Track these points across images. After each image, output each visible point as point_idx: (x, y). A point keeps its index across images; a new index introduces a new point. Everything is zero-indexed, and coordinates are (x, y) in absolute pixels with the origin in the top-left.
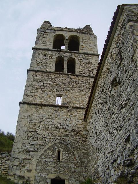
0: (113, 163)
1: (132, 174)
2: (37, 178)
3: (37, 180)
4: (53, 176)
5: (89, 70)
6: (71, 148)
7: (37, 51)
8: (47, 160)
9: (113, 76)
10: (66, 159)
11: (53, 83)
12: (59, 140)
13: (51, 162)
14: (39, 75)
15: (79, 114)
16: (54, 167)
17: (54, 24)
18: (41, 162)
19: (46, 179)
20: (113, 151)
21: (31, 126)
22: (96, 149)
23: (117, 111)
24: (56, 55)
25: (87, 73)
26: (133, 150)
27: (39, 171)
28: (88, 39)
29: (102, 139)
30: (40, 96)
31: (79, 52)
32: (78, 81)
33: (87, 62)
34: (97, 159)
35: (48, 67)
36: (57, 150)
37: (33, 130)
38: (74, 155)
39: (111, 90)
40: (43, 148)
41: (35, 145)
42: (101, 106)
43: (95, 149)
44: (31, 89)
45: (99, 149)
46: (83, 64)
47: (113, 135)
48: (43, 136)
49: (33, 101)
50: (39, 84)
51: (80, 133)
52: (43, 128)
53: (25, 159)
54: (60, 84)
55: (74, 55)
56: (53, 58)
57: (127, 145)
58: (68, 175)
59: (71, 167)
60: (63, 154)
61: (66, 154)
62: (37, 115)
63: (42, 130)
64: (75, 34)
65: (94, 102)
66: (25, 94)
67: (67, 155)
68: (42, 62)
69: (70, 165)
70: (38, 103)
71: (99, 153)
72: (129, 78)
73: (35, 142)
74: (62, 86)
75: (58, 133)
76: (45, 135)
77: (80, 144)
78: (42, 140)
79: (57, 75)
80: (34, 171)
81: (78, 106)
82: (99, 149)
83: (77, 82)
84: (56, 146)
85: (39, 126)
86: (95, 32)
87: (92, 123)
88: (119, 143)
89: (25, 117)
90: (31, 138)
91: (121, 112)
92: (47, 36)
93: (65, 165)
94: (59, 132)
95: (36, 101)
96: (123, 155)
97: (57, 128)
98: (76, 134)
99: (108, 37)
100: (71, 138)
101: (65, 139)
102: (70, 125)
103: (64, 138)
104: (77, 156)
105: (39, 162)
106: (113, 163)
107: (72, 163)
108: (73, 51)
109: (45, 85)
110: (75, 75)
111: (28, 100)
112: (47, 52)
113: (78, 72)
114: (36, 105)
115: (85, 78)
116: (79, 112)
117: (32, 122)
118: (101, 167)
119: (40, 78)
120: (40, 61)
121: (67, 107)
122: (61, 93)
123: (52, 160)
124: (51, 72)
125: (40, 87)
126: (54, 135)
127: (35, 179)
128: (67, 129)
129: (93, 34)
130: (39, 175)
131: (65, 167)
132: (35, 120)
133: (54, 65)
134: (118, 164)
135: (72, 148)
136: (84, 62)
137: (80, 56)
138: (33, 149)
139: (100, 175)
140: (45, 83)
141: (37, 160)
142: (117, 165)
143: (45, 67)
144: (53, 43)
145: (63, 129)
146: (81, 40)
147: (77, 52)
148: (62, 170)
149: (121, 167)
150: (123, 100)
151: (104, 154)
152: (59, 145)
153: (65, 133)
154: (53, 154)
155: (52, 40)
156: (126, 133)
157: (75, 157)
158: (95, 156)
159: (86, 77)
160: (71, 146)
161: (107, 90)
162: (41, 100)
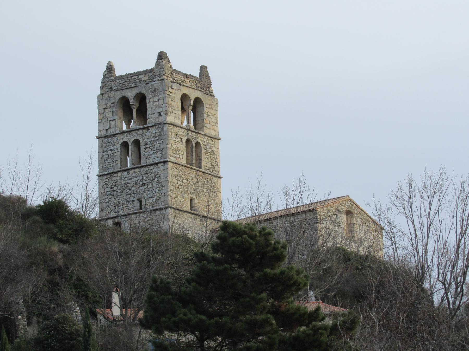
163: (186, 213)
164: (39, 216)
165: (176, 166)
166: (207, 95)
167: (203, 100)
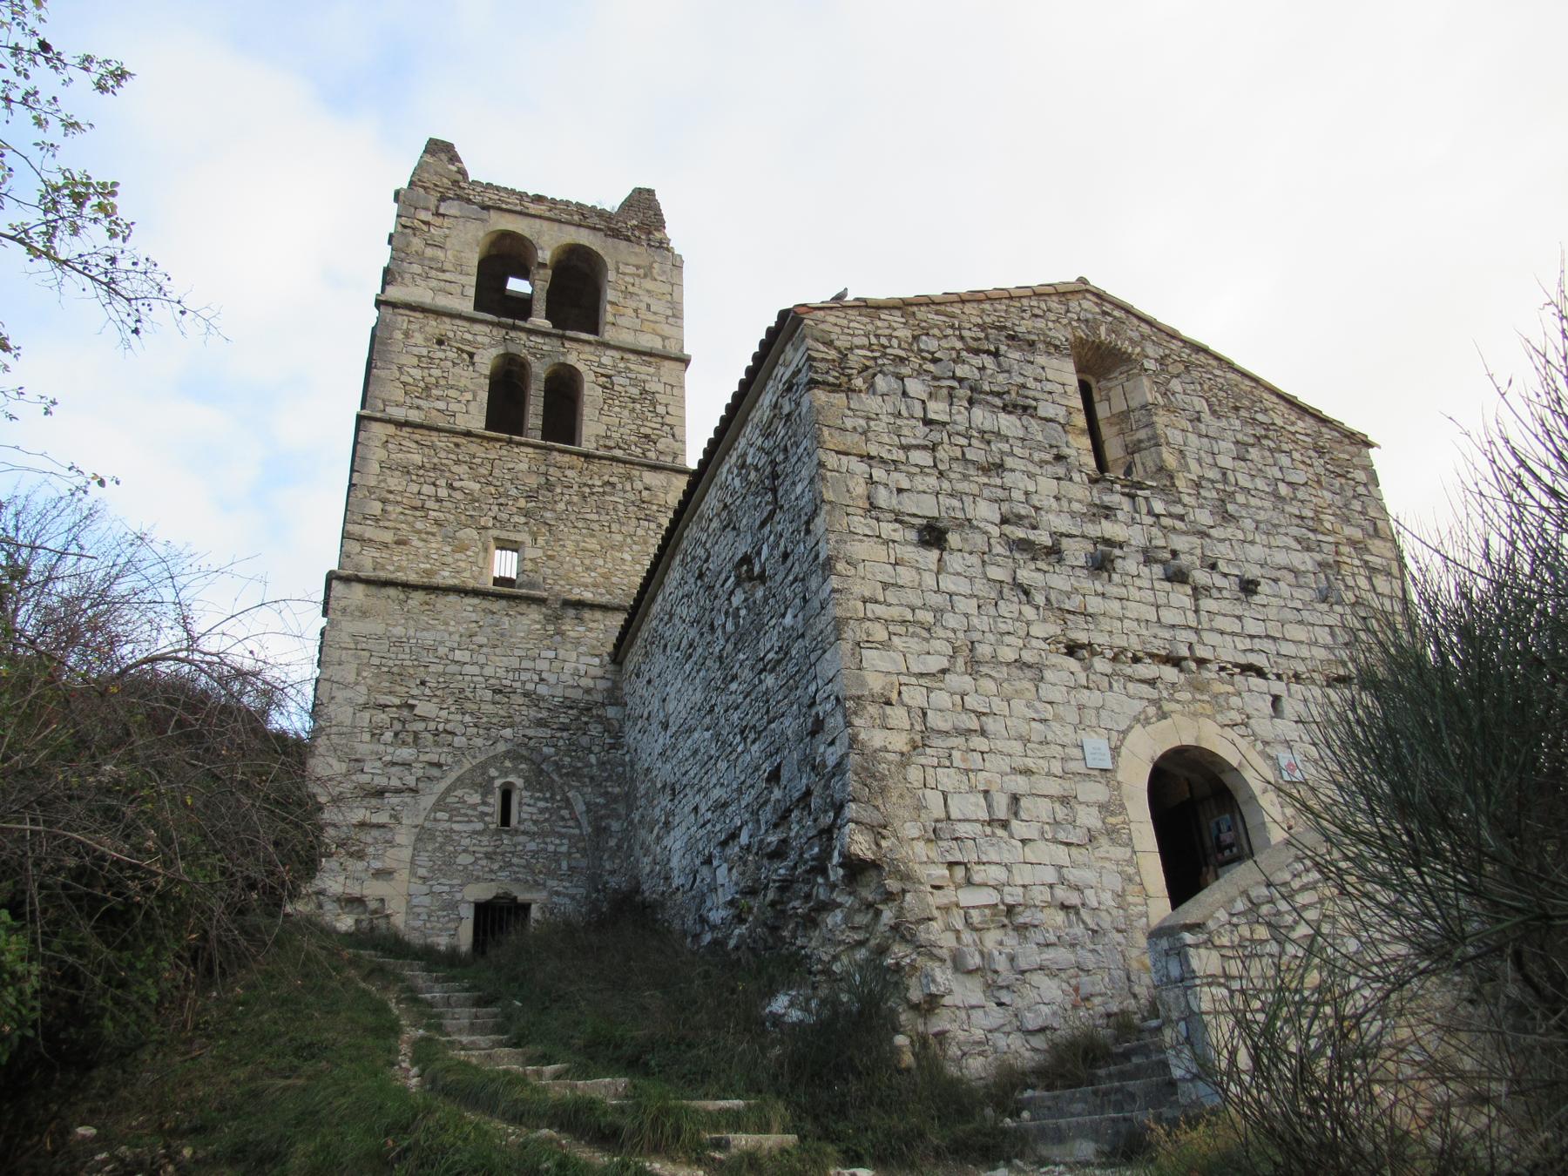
0: (724, 844)
1: (779, 881)
2: (415, 901)
3: (416, 910)
4: (484, 892)
5: (642, 430)
6: (555, 777)
7: (400, 318)
8: (456, 827)
9: (743, 548)
10: (535, 822)
11: (478, 486)
12: (506, 740)
13: (475, 832)
14: (414, 445)
15: (590, 630)
16: (488, 856)
17: (481, 166)
18: (433, 838)
19: (453, 906)
20: (725, 805)
21: (387, 684)
22: (664, 787)
23: (746, 674)
24: (492, 346)
25: (633, 447)
26: (789, 811)
27: (422, 872)
28: (641, 272)
29: (688, 754)
30: (421, 544)
31: (596, 338)
32: (590, 482)
33: (635, 391)
34: (667, 823)
35: (454, 407)
36: (498, 783)
37: (397, 701)
38: (568, 803)
39: (732, 593)
40: (439, 779)
41: (407, 765)
42: (693, 633)
43: (659, 785)
44: (378, 512)
45: (673, 790)
46: (617, 402)
47: (730, 749)
48: (441, 727)
49: (392, 568)
50: (415, 488)
51: (594, 712)
52: (438, 693)
53: (362, 825)
54: (513, 492)
55: (575, 354)
56: (476, 359)
57: (771, 792)
58: (544, 885)
59: (555, 853)
60: (524, 801)
61: (538, 799)
62: (411, 632)
63: (435, 700)
64: (584, 238)
65: (660, 598)
66: (346, 535)
67: (542, 804)
68: (428, 379)
69: (553, 844)
70: (413, 578)
71: (676, 802)
72: (792, 584)
73: (406, 753)
74: (522, 503)
75: (502, 713)
76: (448, 721)
77: (593, 759)
78: (436, 744)
79: (498, 445)
80: (403, 875)
81: (588, 596)
82: (677, 786)
83: (585, 485)
84: (497, 769)
85: (423, 683)
86: (674, 231)
87: (649, 682)
88: (749, 782)
89: (356, 644)
90: (388, 736)
91: (761, 682)
92: (446, 237)
93: (532, 846)
94: (506, 706)
95: (400, 568)
96: (758, 821)
97: (500, 692)
98: (578, 718)
99: (738, 398)
100: (559, 735)
101: (530, 739)
102: (552, 679)
103: (531, 733)
104: (580, 807)
105: (423, 835)
106: (724, 844)
107: (562, 836)
108: (570, 333)
109: (443, 493)
110: (579, 454)
111: (367, 562)
112: (446, 326)
113: (593, 439)
114: (406, 586)
115: (619, 469)
116: (591, 625)
117: (391, 663)
118: (681, 853)
119: (417, 459)
120: (417, 373)
121: (541, 601)
122: (513, 536)
123: (479, 826)
124: (468, 434)
125: (419, 504)
126: (485, 720)
127: (410, 908)
128: (542, 698)
129: (663, 246)
130: (425, 889)
131: (535, 854)
132: (400, 656)
133: (484, 396)
134: (741, 848)
135: (561, 776)
136: (620, 389)
137: (605, 360)
138: (395, 783)
139: (676, 882)
140: (442, 482)
141: (416, 827)
142: (737, 849)
143: (441, 405)
144: (474, 279)
145: (526, 694)
146: (611, 276)
147: (591, 337)
148: (518, 866)
149: (750, 858)
150: (768, 646)
151: (696, 809)
152: (508, 764)
153: (533, 713)
154: (484, 803)
155: (473, 259)
156: (771, 756)
157: (572, 812)
158: (657, 810)
159: (625, 462)
160: (558, 766)
161: (718, 586)
162: (428, 566)
163: (452, 598)
164: (602, 685)
165: (417, 437)
166: (624, 243)
167: (601, 252)
